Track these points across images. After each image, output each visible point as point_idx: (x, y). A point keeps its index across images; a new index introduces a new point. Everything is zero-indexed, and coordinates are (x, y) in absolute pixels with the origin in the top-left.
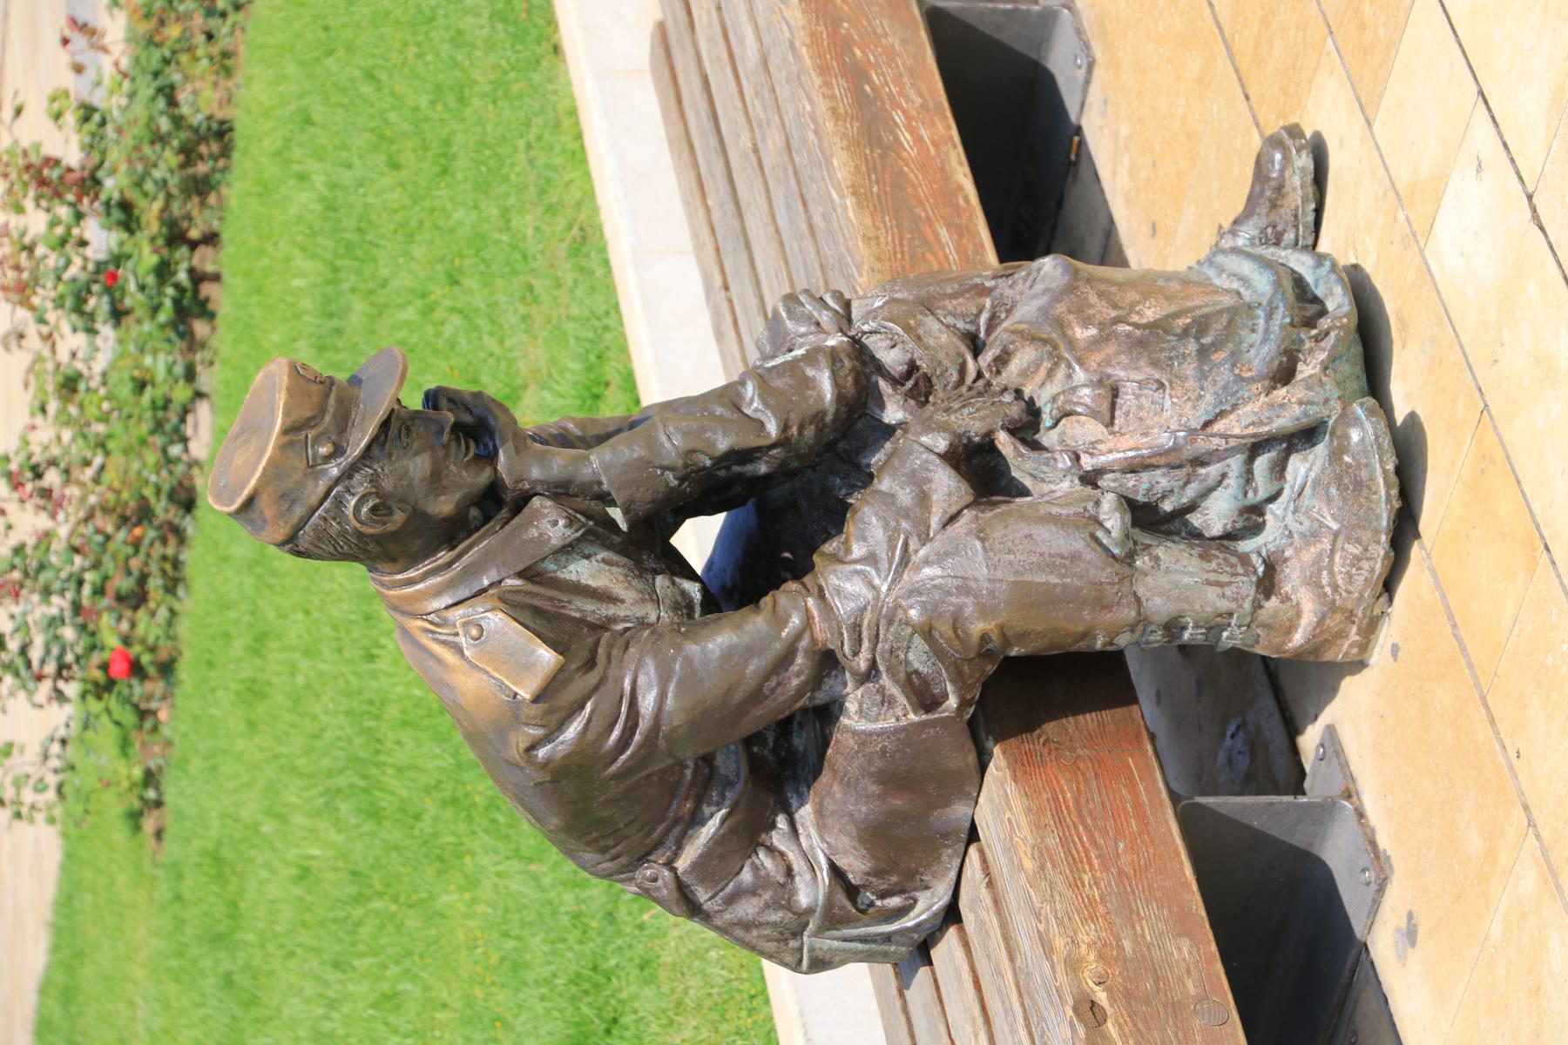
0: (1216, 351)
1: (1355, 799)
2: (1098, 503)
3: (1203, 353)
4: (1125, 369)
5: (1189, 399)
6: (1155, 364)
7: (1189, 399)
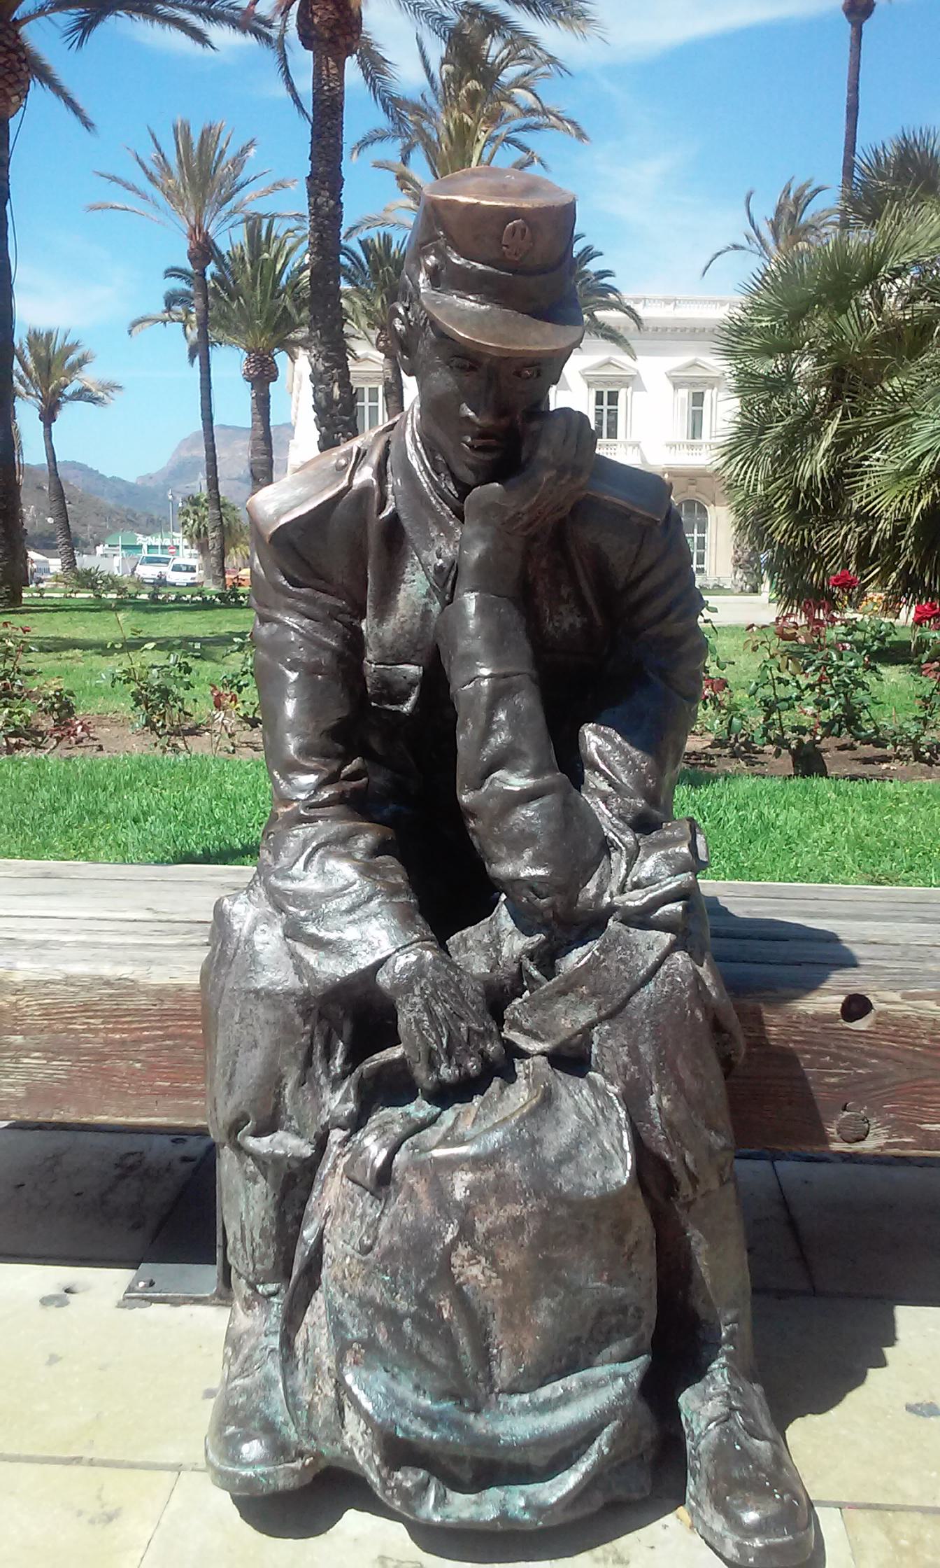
0: (388, 1331)
1: (216, 1300)
2: (298, 1134)
3: (392, 1317)
4: (396, 1215)
5: (344, 1277)
6: (390, 1253)
7: (344, 1277)
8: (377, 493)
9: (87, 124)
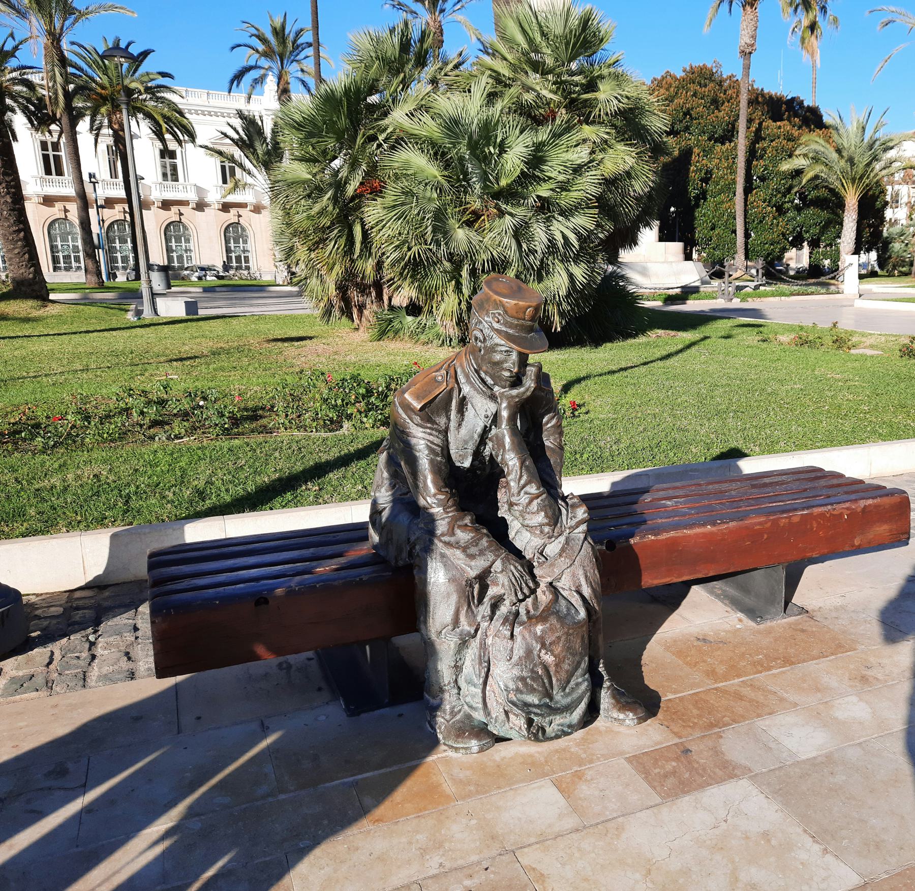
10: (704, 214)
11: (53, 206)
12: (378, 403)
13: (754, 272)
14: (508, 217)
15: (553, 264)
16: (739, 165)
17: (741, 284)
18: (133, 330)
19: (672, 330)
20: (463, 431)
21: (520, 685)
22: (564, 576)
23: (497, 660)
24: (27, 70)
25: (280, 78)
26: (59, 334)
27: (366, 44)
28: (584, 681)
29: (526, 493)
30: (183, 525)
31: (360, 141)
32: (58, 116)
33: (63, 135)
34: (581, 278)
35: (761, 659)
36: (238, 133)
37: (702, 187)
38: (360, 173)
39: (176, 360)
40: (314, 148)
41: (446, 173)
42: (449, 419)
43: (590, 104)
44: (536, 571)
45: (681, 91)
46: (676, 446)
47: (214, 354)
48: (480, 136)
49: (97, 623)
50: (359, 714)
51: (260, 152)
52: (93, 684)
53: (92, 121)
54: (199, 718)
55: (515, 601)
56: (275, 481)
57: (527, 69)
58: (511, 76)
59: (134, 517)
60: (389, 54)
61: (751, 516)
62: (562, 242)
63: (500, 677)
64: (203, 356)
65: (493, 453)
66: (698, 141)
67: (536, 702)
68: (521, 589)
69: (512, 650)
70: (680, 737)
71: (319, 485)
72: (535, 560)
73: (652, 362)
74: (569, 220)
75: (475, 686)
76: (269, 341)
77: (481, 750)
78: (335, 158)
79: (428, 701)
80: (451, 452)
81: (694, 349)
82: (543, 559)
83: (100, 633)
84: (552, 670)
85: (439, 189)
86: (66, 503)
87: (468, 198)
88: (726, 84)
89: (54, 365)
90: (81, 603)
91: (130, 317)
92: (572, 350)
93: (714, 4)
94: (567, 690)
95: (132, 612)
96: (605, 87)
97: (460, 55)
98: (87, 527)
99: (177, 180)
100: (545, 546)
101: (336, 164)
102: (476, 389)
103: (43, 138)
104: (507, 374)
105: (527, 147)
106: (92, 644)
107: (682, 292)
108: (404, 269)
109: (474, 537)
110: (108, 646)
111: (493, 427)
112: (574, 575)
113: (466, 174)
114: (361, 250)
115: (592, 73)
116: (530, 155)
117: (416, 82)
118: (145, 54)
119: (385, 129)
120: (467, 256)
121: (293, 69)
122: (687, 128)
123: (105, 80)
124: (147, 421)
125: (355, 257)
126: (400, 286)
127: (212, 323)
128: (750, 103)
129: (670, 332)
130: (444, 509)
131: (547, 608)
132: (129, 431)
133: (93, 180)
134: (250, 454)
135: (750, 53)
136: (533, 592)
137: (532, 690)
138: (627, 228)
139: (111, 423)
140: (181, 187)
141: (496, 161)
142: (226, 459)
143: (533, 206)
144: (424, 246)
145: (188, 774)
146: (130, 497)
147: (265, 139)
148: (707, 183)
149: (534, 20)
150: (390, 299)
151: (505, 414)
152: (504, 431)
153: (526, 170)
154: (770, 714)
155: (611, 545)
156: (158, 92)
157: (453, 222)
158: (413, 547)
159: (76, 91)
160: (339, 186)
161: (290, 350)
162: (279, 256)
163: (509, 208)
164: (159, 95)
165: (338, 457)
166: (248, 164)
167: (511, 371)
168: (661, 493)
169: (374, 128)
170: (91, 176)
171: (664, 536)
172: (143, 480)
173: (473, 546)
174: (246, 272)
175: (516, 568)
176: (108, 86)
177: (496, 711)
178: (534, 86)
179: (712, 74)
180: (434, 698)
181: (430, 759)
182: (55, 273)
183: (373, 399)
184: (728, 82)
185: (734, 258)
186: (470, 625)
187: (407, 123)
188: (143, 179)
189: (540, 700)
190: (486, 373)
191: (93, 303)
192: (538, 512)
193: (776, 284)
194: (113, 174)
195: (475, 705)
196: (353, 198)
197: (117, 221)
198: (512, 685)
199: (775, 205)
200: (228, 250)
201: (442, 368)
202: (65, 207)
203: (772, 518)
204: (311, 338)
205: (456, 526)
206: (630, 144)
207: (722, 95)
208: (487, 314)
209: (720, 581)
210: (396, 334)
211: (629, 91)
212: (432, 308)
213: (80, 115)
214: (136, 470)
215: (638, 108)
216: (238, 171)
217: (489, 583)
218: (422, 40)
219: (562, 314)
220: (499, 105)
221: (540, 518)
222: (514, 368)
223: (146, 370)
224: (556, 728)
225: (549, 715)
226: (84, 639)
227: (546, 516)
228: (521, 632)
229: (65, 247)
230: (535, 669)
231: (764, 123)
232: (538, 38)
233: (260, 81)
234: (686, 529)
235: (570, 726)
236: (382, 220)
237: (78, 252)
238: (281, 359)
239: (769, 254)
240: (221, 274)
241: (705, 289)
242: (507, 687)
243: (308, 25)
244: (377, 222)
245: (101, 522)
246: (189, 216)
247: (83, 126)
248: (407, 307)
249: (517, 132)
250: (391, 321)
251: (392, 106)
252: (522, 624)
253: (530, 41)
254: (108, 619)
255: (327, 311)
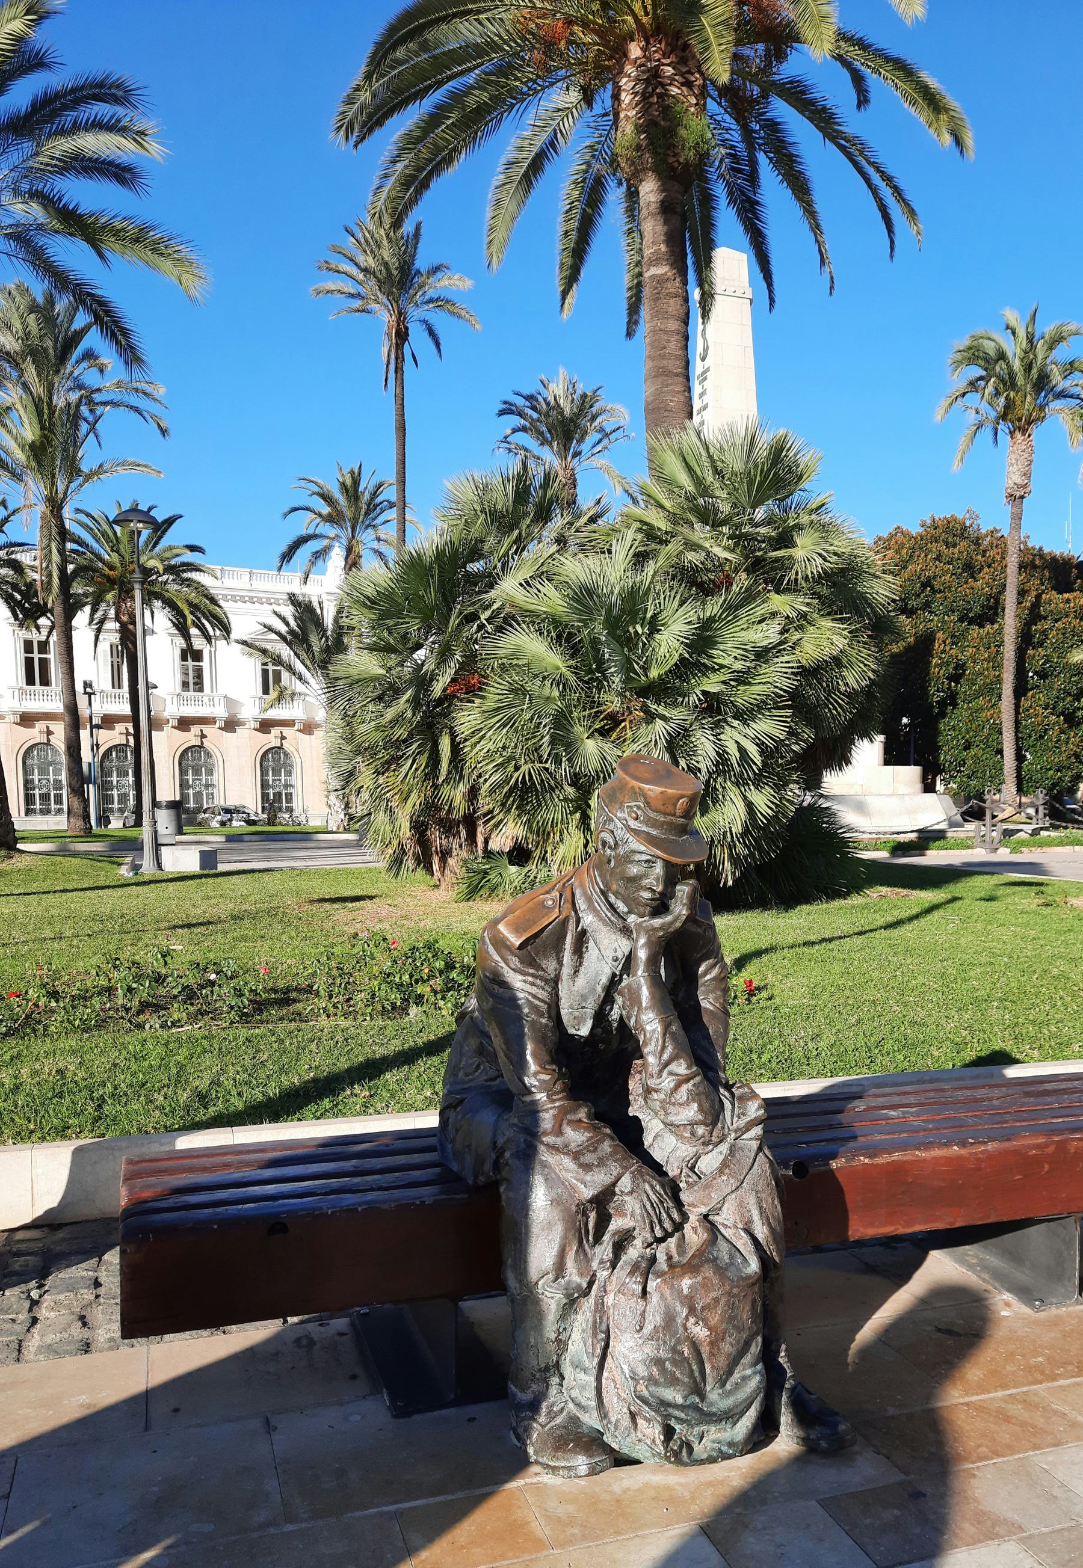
8: (510, 917)
9: (892, 257)
10: (953, 726)
11: (33, 727)
12: (461, 979)
13: (1031, 811)
14: (659, 722)
15: (724, 788)
16: (1006, 656)
17: (1011, 827)
18: (125, 889)
19: (904, 887)
20: (581, 981)
21: (655, 1371)
22: (726, 1205)
23: (621, 1331)
24: (16, 549)
25: (349, 550)
26: (25, 894)
27: (469, 494)
28: (755, 1373)
29: (671, 1074)
30: (175, 1139)
31: (454, 621)
32: (50, 605)
33: (54, 632)
34: (764, 809)
35: (1041, 1363)
36: (287, 624)
37: (949, 688)
38: (452, 665)
39: (182, 927)
40: (390, 633)
41: (570, 663)
42: (560, 963)
43: (784, 565)
44: (684, 1197)
45: (917, 553)
46: (907, 1045)
47: (234, 918)
48: (623, 610)
49: (42, 1274)
50: (409, 1415)
51: (316, 649)
52: (31, 1357)
53: (94, 611)
54: (176, 1410)
55: (650, 1240)
56: (308, 1082)
57: (694, 519)
58: (669, 529)
59: (107, 1129)
60: (499, 506)
61: (1023, 1134)
62: (738, 756)
63: (625, 1357)
64: (219, 921)
65: (624, 1013)
66: (944, 622)
67: (680, 1400)
68: (660, 1221)
69: (643, 1314)
70: (907, 1473)
71: (370, 1089)
72: (683, 1179)
73: (871, 931)
74: (748, 726)
75: (585, 1370)
76: (312, 902)
77: (593, 1472)
78: (419, 646)
79: (514, 1395)
80: (563, 1012)
81: (935, 916)
82: (695, 1178)
83: (46, 1288)
84: (705, 1351)
85: (562, 684)
86: (16, 1106)
87: (604, 697)
88: (986, 542)
89: (16, 932)
90: (23, 1247)
91: (124, 872)
92: (749, 914)
93: (967, 432)
94: (728, 1387)
95: (93, 1262)
96: (804, 540)
97: (598, 502)
98: (43, 1139)
99: (201, 690)
100: (697, 1157)
101: (420, 654)
102: (601, 919)
103: (29, 636)
104: (647, 895)
105: (689, 623)
106: (34, 1303)
107: (919, 838)
108: (507, 796)
109: (592, 1138)
110: (57, 1306)
111: (625, 976)
112: (741, 1204)
113: (600, 662)
114: (449, 772)
115: (785, 521)
116: (693, 634)
117: (536, 542)
118: (170, 522)
119: (489, 606)
120: (599, 777)
121: (367, 537)
122: (927, 606)
123: (115, 558)
124: (136, 1002)
125: (440, 781)
126: (501, 821)
127: (235, 879)
128: (1022, 567)
129: (901, 890)
130: (548, 1096)
131: (700, 1253)
132: (111, 1018)
133: (89, 690)
134: (275, 1046)
135: (1022, 497)
136: (678, 1227)
137: (673, 1382)
138: (836, 740)
139: (86, 1007)
140: (206, 700)
141: (644, 644)
142: (241, 1052)
143: (696, 706)
144: (538, 765)
145: (156, 1489)
146: (104, 1101)
147: (325, 631)
148: (957, 683)
149: (704, 453)
150: (486, 841)
151: (642, 954)
152: (640, 981)
153: (687, 655)
154: (1055, 1445)
155: (800, 1169)
156: (184, 571)
157: (579, 730)
158: (501, 1154)
159: (75, 573)
160: (422, 681)
161: (339, 912)
162: (336, 784)
163: (661, 710)
164: (185, 575)
165: (399, 1052)
166: (299, 666)
167: (653, 891)
168: (881, 1099)
169: (474, 603)
170: (87, 685)
171: (883, 1159)
172: (123, 1079)
173: (589, 1151)
174: (287, 816)
175: (652, 1187)
176: (118, 565)
177: (617, 1410)
178: (701, 542)
179: (965, 528)
180: (523, 1390)
181: (512, 1485)
182: (28, 818)
183: (454, 975)
184: (988, 539)
185: (999, 791)
186: (581, 1275)
187: (521, 597)
188: (156, 687)
189: (685, 1398)
190: (616, 894)
191: (76, 855)
192: (687, 1103)
193: (1066, 828)
194: (117, 683)
195: (584, 1402)
196: (440, 701)
197: (116, 746)
198: (642, 1371)
199: (1062, 713)
200: (264, 785)
201: (553, 888)
202: (48, 728)
203: (1056, 1139)
204: (371, 898)
205: (565, 1122)
206: (841, 619)
207: (979, 557)
208: (621, 808)
209: (975, 1245)
210: (493, 891)
211: (840, 545)
212: (546, 852)
213: (78, 606)
214: (115, 1065)
215: (853, 569)
216: (285, 675)
217: (611, 1211)
218: (546, 485)
219: (735, 860)
220: (650, 568)
221: (691, 1112)
222: (657, 885)
223: (140, 939)
224: (710, 1445)
225: (699, 1423)
226: (23, 1296)
227: (701, 1109)
228: (658, 1287)
229: (44, 782)
230: (679, 1348)
231: (1044, 596)
232: (709, 477)
233: (321, 554)
234: (919, 1149)
235: (731, 1444)
236: (480, 730)
237: (61, 789)
238: (328, 925)
239: (1054, 785)
240: (253, 818)
241: (955, 834)
242: (635, 1374)
243: (392, 477)
244: (473, 733)
245: (61, 1132)
246: (216, 739)
247: (81, 619)
248: (510, 853)
249: (676, 603)
250: (486, 873)
251: (501, 574)
252: (660, 1274)
253: (698, 481)
254: (59, 1270)
255: (396, 860)
